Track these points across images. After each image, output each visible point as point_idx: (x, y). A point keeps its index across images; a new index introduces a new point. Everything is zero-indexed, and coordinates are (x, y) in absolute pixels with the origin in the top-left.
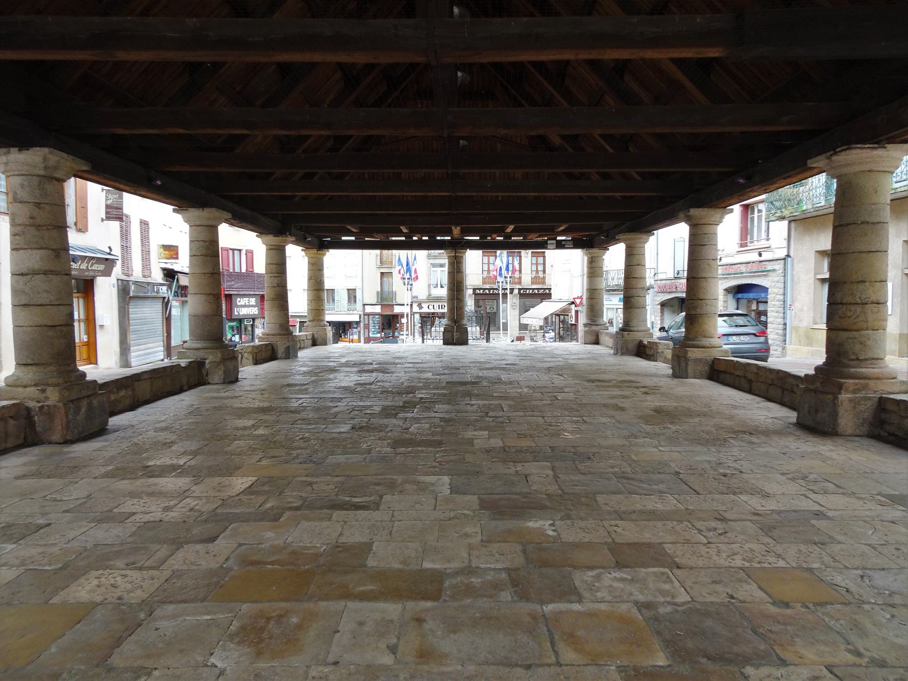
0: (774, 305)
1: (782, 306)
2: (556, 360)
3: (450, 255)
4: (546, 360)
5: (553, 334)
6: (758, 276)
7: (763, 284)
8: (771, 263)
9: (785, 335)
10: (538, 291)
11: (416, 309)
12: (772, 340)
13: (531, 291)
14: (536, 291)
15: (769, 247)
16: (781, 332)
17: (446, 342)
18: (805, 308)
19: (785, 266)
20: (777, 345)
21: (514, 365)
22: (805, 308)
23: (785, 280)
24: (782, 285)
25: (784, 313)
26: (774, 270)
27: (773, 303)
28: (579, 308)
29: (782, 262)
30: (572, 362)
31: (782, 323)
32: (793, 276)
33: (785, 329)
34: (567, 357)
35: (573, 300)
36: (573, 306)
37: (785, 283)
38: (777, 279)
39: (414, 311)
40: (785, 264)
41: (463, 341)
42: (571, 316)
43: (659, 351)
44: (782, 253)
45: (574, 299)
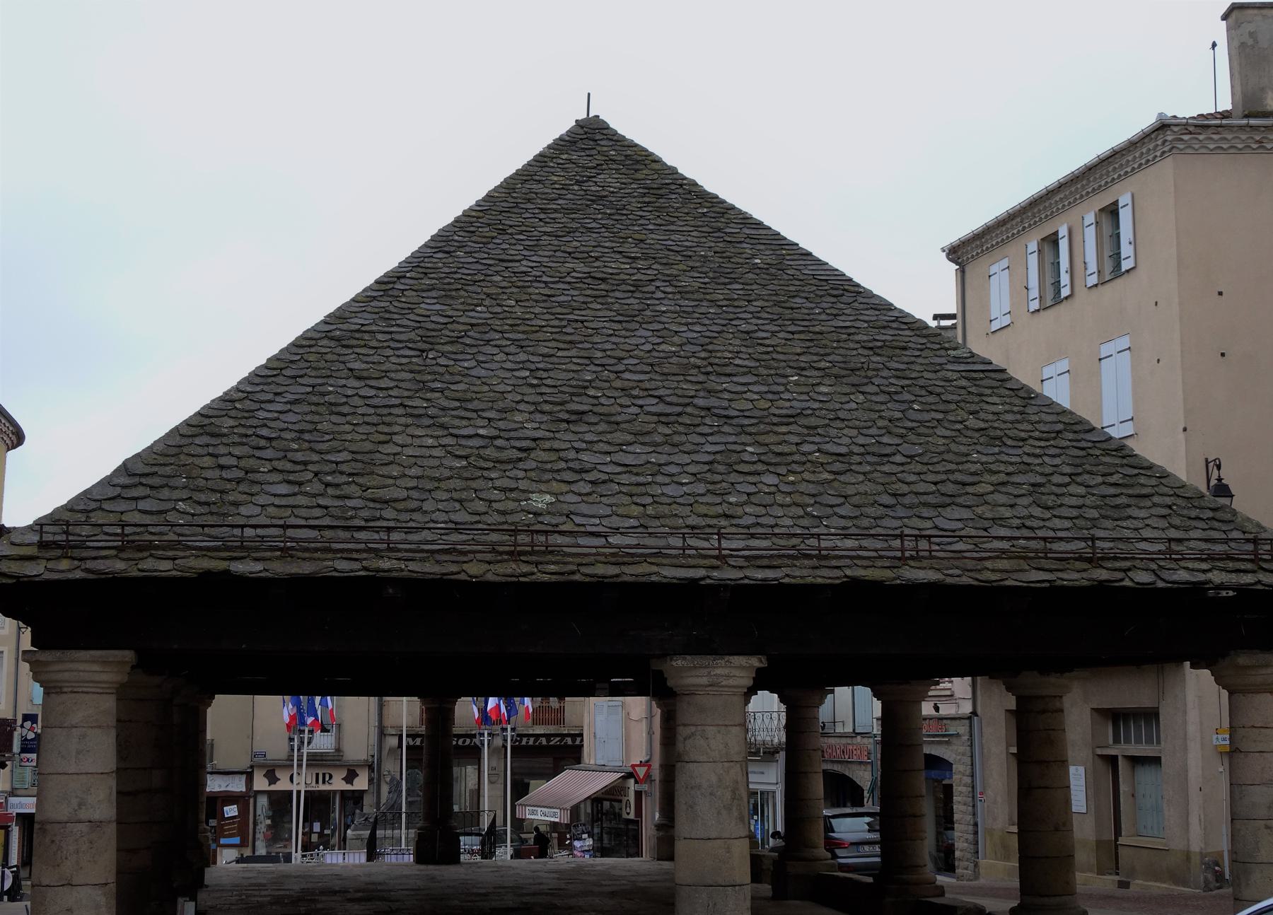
0: (961, 792)
1: (971, 795)
2: (618, 883)
3: (429, 706)
4: (603, 883)
5: (590, 842)
6: (939, 743)
7: (946, 757)
8: (954, 722)
9: (976, 843)
10: (548, 741)
11: (260, 783)
12: (961, 851)
13: (532, 739)
14: (544, 741)
15: (952, 696)
16: (971, 837)
17: (421, 858)
18: (999, 799)
19: (971, 729)
20: (967, 861)
21: (560, 889)
22: (999, 799)
23: (972, 753)
24: (968, 760)
25: (974, 806)
26: (958, 735)
27: (960, 789)
28: (645, 787)
29: (967, 721)
30: (642, 885)
31: (972, 822)
32: (982, 747)
33: (976, 833)
34: (634, 879)
35: (630, 770)
36: (632, 781)
37: (972, 756)
38: (961, 749)
39: (256, 788)
40: (971, 726)
41: (452, 856)
42: (628, 803)
43: (764, 867)
44: (967, 708)
45: (633, 766)
